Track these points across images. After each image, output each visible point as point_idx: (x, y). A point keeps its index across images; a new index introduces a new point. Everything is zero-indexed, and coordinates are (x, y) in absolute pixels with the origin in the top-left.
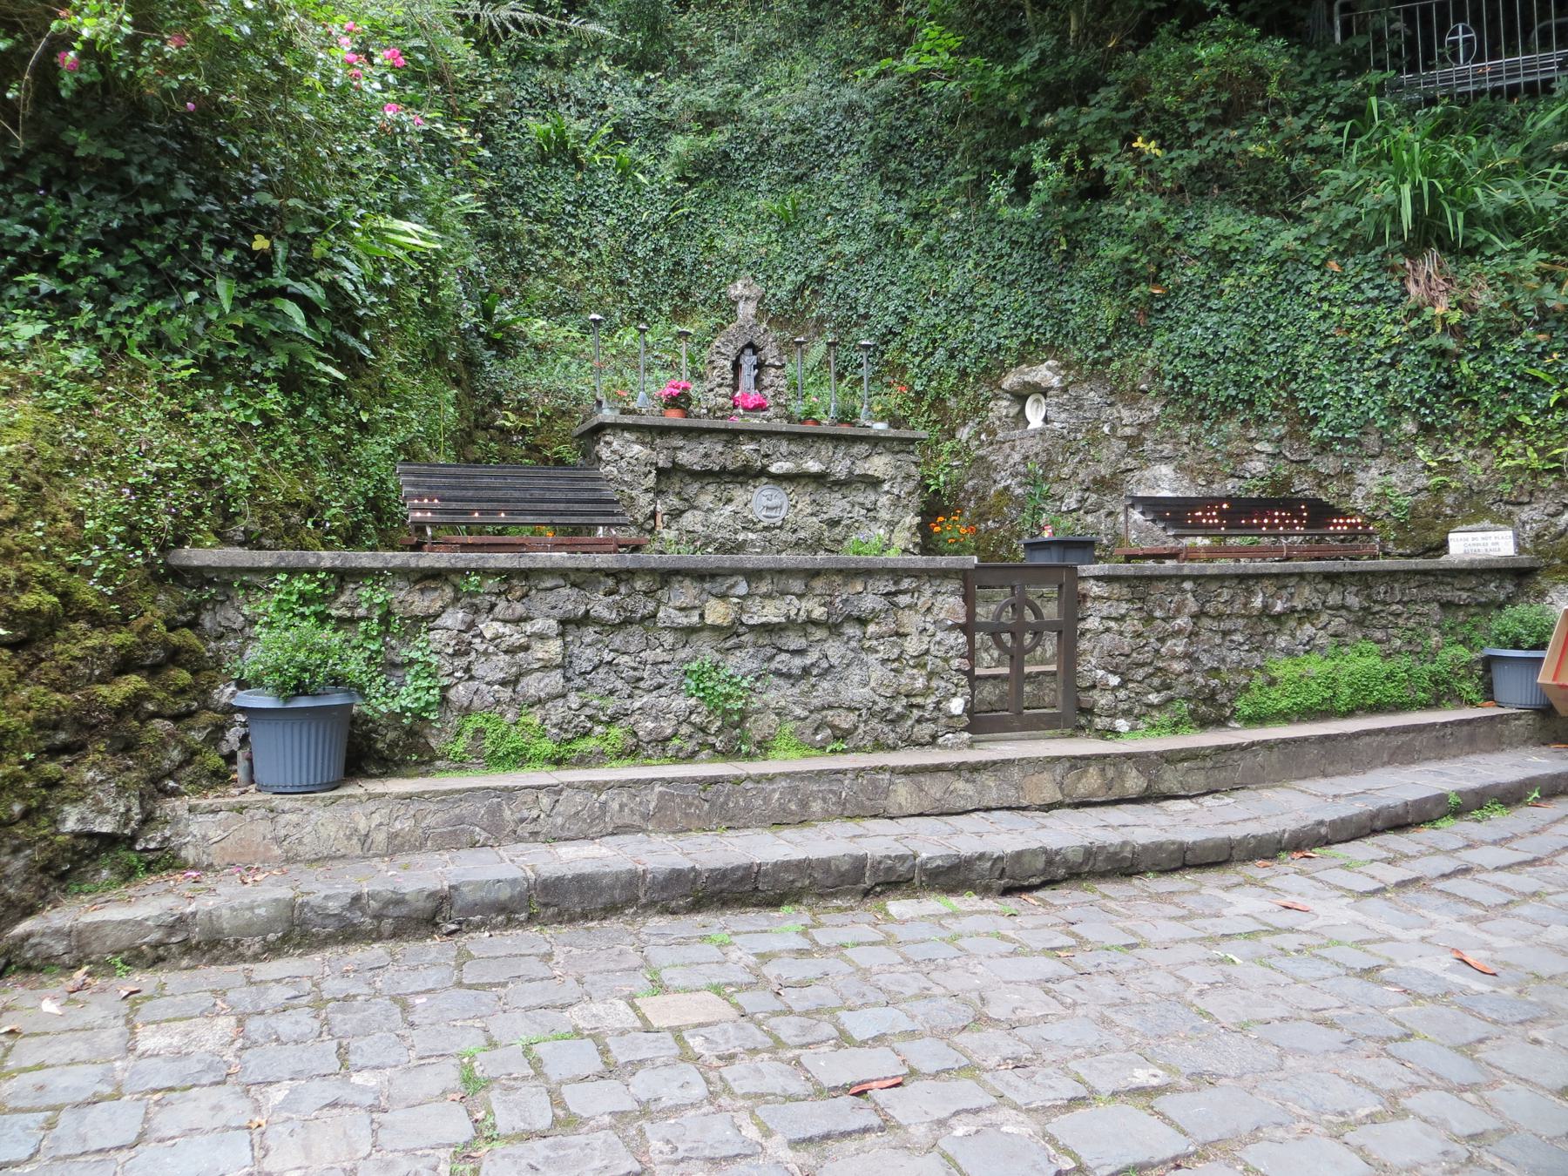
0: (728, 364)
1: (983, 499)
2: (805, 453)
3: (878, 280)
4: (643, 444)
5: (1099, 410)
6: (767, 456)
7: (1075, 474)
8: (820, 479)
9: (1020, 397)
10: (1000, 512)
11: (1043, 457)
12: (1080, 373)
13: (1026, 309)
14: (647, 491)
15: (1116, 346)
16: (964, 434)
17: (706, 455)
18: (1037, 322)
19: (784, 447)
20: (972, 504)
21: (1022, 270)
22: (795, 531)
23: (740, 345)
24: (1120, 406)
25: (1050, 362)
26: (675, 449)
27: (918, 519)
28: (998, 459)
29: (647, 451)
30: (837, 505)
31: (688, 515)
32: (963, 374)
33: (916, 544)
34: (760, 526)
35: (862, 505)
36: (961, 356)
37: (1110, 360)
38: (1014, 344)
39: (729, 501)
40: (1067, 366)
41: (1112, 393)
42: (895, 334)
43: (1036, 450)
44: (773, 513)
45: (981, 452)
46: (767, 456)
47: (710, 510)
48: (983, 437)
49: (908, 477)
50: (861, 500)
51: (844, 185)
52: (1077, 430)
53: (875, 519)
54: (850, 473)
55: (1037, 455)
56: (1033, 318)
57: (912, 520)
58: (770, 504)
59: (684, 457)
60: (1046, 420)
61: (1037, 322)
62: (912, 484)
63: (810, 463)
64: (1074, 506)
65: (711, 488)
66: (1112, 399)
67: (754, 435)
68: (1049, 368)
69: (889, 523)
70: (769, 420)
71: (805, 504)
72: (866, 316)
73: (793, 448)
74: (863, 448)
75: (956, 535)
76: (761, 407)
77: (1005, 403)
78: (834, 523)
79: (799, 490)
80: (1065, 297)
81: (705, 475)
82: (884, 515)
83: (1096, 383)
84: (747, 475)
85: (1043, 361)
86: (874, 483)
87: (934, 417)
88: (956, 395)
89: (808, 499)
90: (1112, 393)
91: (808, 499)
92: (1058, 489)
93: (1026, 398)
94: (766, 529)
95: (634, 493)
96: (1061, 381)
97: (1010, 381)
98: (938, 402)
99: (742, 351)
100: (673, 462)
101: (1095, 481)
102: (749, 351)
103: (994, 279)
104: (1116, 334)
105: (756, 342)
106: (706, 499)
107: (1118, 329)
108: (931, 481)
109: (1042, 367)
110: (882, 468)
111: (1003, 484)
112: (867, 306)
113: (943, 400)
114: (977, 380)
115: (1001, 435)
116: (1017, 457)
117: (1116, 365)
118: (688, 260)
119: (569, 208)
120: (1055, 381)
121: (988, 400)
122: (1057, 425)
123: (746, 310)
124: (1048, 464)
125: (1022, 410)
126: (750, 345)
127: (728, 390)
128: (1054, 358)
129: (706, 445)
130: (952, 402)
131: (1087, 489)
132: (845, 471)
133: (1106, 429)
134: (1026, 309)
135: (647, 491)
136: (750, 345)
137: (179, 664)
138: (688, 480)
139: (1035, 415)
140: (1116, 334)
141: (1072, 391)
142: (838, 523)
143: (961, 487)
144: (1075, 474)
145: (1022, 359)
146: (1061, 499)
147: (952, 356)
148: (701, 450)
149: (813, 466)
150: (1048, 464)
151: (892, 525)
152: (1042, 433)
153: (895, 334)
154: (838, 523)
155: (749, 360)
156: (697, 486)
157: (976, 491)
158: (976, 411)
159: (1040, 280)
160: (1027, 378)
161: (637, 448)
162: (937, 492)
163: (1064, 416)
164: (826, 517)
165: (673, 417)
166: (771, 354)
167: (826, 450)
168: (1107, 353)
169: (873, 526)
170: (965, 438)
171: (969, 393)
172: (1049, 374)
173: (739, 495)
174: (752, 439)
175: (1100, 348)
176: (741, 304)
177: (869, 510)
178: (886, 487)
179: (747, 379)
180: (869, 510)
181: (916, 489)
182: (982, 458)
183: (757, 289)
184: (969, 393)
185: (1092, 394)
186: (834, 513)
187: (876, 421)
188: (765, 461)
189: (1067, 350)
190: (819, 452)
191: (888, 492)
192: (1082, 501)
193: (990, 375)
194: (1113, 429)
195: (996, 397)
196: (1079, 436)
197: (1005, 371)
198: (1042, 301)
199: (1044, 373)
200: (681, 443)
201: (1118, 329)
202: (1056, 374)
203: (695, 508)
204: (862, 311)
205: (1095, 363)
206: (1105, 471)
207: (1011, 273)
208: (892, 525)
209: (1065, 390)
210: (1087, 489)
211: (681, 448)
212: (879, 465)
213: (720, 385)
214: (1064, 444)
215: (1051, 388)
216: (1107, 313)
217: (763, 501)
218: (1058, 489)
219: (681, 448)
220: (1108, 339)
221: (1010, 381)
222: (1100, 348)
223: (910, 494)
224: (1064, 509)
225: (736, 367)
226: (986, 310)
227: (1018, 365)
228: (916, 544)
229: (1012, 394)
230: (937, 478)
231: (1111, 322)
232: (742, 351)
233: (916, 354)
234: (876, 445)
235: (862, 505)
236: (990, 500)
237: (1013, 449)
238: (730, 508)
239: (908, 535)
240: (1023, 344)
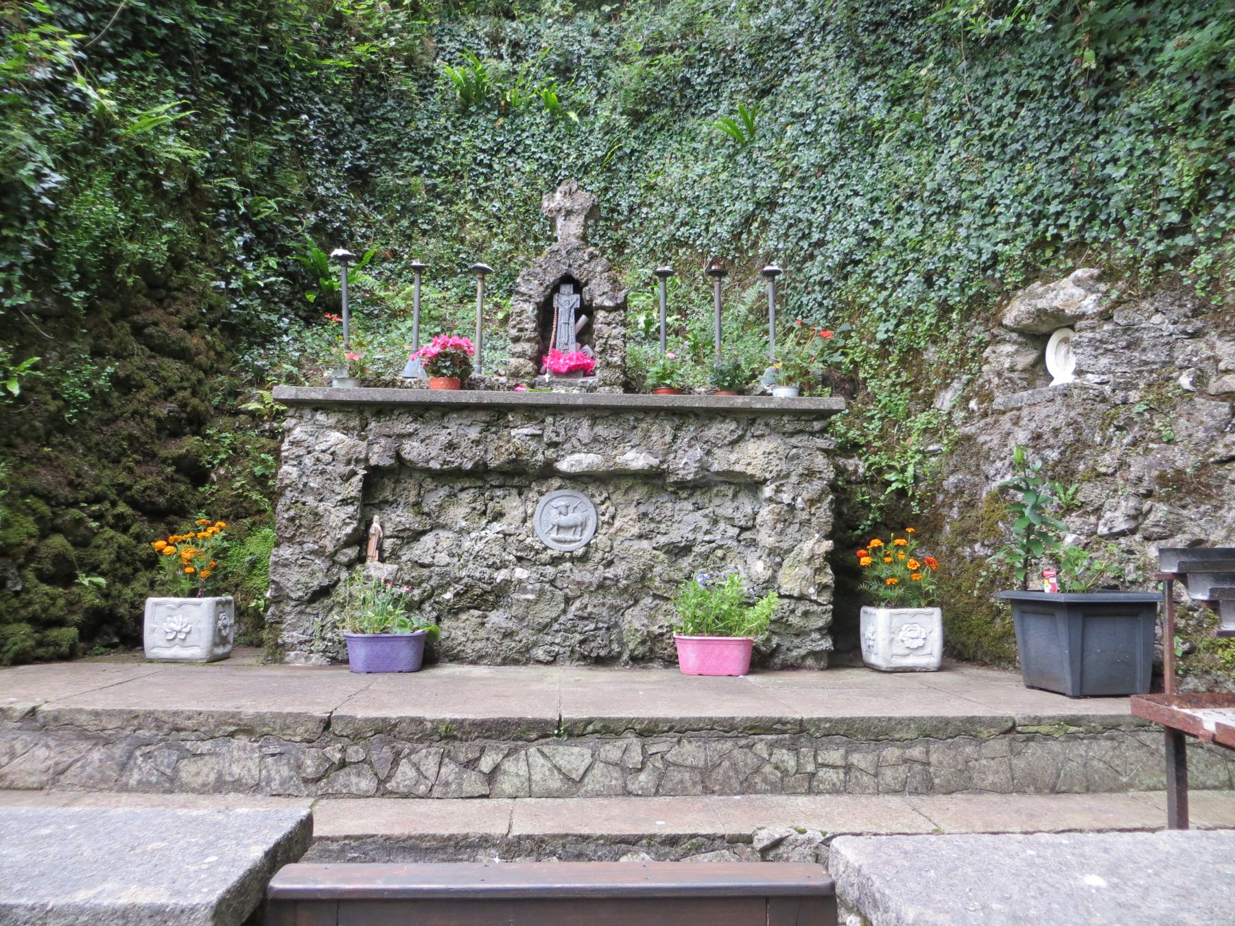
0: (530, 308)
1: (970, 505)
2: (622, 439)
3: (837, 192)
4: (346, 430)
5: (1171, 346)
6: (554, 445)
7: (1123, 465)
8: (653, 479)
9: (1035, 337)
10: (992, 529)
11: (1067, 435)
12: (1133, 284)
13: (1035, 192)
14: (345, 502)
15: (1200, 224)
16: (946, 400)
17: (451, 446)
18: (1054, 207)
19: (584, 431)
20: (955, 513)
21: (1033, 133)
22: (610, 564)
23: (550, 279)
24: (1213, 335)
25: (1079, 273)
26: (401, 436)
27: (828, 545)
28: (990, 439)
29: (349, 441)
30: (684, 521)
31: (428, 540)
32: (945, 309)
33: (822, 588)
34: (544, 557)
35: (730, 520)
36: (941, 282)
37: (1193, 253)
38: (1016, 250)
39: (498, 516)
40: (1109, 275)
41: (1196, 313)
42: (856, 263)
43: (1055, 423)
44: (568, 536)
45: (969, 430)
46: (554, 445)
47: (461, 531)
48: (973, 404)
49: (810, 474)
50: (729, 512)
51: (812, 85)
52: (1129, 386)
53: (753, 543)
54: (704, 468)
55: (1056, 431)
56: (1048, 202)
57: (817, 545)
58: (563, 520)
59: (413, 450)
60: (1079, 372)
61: (1054, 207)
62: (817, 485)
63: (631, 455)
64: (1121, 525)
65: (466, 497)
66: (1198, 323)
67: (532, 412)
68: (1078, 282)
69: (772, 552)
70: (592, 389)
71: (627, 520)
72: (821, 243)
73: (600, 430)
74: (726, 429)
75: (899, 570)
76: (586, 370)
77: (1009, 348)
78: (678, 551)
79: (618, 497)
80: (1102, 157)
81: (450, 476)
82: (766, 538)
83: (1163, 298)
84: (522, 475)
85: (1068, 272)
86: (752, 485)
87: (904, 376)
88: (934, 342)
89: (633, 512)
90: (1196, 313)
91: (633, 512)
92: (1090, 492)
93: (1047, 337)
94: (555, 561)
95: (321, 508)
96: (1099, 302)
97: (1016, 311)
98: (910, 356)
99: (556, 288)
100: (398, 456)
101: (1162, 480)
102: (567, 289)
103: (990, 157)
104: (1200, 201)
105: (576, 274)
106: (458, 514)
107: (1203, 194)
108: (891, 476)
109: (1067, 282)
110: (760, 461)
111: (999, 482)
112: (823, 229)
113: (918, 352)
114: (966, 316)
115: (999, 401)
116: (1022, 436)
117: (1204, 259)
118: (624, 205)
119: (481, 156)
120: (1089, 304)
121: (982, 345)
122: (1092, 379)
123: (569, 230)
124: (1078, 447)
125: (1041, 359)
126: (567, 279)
127: (529, 348)
128: (1089, 263)
129: (454, 429)
130: (931, 354)
131: (1149, 494)
132: (693, 468)
133: (1185, 381)
134: (1035, 192)
135: (345, 502)
136: (567, 279)
137: (904, 527)
138: (429, 484)
139: (1061, 364)
140: (1200, 201)
141: (1120, 318)
142: (687, 549)
143: (937, 487)
144: (1123, 465)
145: (1032, 273)
146: (1098, 511)
147: (928, 280)
148: (443, 437)
149: (636, 459)
150: (1078, 447)
151: (777, 555)
152: (1066, 393)
153: (856, 263)
154: (687, 549)
155: (566, 301)
156: (442, 492)
157: (960, 492)
158: (962, 362)
159: (1061, 141)
160: (1042, 304)
161: (335, 436)
162: (901, 493)
163: (1104, 361)
164: (662, 540)
165: (440, 391)
166: (599, 292)
167: (660, 433)
168: (1184, 241)
169: (751, 555)
170: (947, 406)
171: (954, 337)
172: (1079, 292)
173: (513, 506)
174: (530, 419)
175: (1170, 232)
176: (560, 222)
177: (743, 529)
178: (768, 491)
179: (565, 329)
180: (743, 529)
181: (823, 493)
182: (969, 438)
183: (583, 200)
184: (954, 337)
185: (1157, 319)
186: (677, 534)
187: (779, 383)
188: (550, 453)
189: (1106, 245)
190: (646, 436)
191: (770, 500)
192: (1137, 516)
193: (981, 305)
194: (1200, 379)
195: (996, 340)
196: (1134, 396)
197: (1008, 296)
198: (1065, 172)
199: (1070, 292)
200: (410, 428)
201: (1203, 194)
202: (1090, 290)
203: (444, 527)
204: (816, 236)
205: (1160, 260)
206: (1184, 460)
207: (1014, 141)
208: (777, 555)
209: (1106, 316)
210: (1149, 494)
211: (410, 435)
212: (754, 455)
213: (516, 340)
214: (1102, 410)
215: (1082, 316)
216: (1179, 171)
217: (554, 518)
218: (1090, 492)
219: (410, 435)
220: (1186, 215)
221: (1016, 311)
222: (1170, 232)
223: (812, 502)
224: (1103, 530)
225: (546, 314)
226: (977, 204)
227: (1027, 282)
228: (822, 588)
229: (1021, 332)
230: (903, 470)
231: (1188, 181)
232: (556, 288)
233: (882, 287)
234: (752, 422)
235: (730, 520)
236: (982, 508)
237: (1016, 422)
238: (497, 526)
239: (808, 571)
240: (1033, 247)
